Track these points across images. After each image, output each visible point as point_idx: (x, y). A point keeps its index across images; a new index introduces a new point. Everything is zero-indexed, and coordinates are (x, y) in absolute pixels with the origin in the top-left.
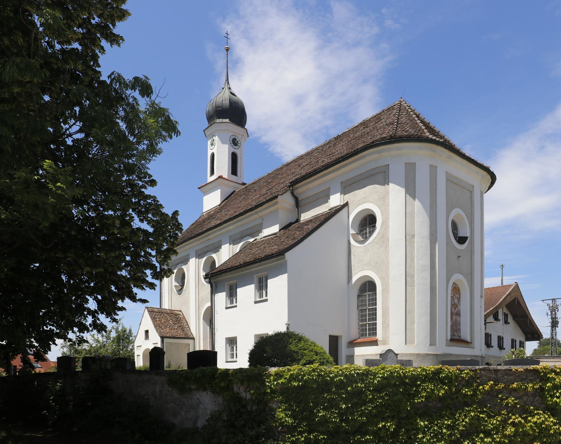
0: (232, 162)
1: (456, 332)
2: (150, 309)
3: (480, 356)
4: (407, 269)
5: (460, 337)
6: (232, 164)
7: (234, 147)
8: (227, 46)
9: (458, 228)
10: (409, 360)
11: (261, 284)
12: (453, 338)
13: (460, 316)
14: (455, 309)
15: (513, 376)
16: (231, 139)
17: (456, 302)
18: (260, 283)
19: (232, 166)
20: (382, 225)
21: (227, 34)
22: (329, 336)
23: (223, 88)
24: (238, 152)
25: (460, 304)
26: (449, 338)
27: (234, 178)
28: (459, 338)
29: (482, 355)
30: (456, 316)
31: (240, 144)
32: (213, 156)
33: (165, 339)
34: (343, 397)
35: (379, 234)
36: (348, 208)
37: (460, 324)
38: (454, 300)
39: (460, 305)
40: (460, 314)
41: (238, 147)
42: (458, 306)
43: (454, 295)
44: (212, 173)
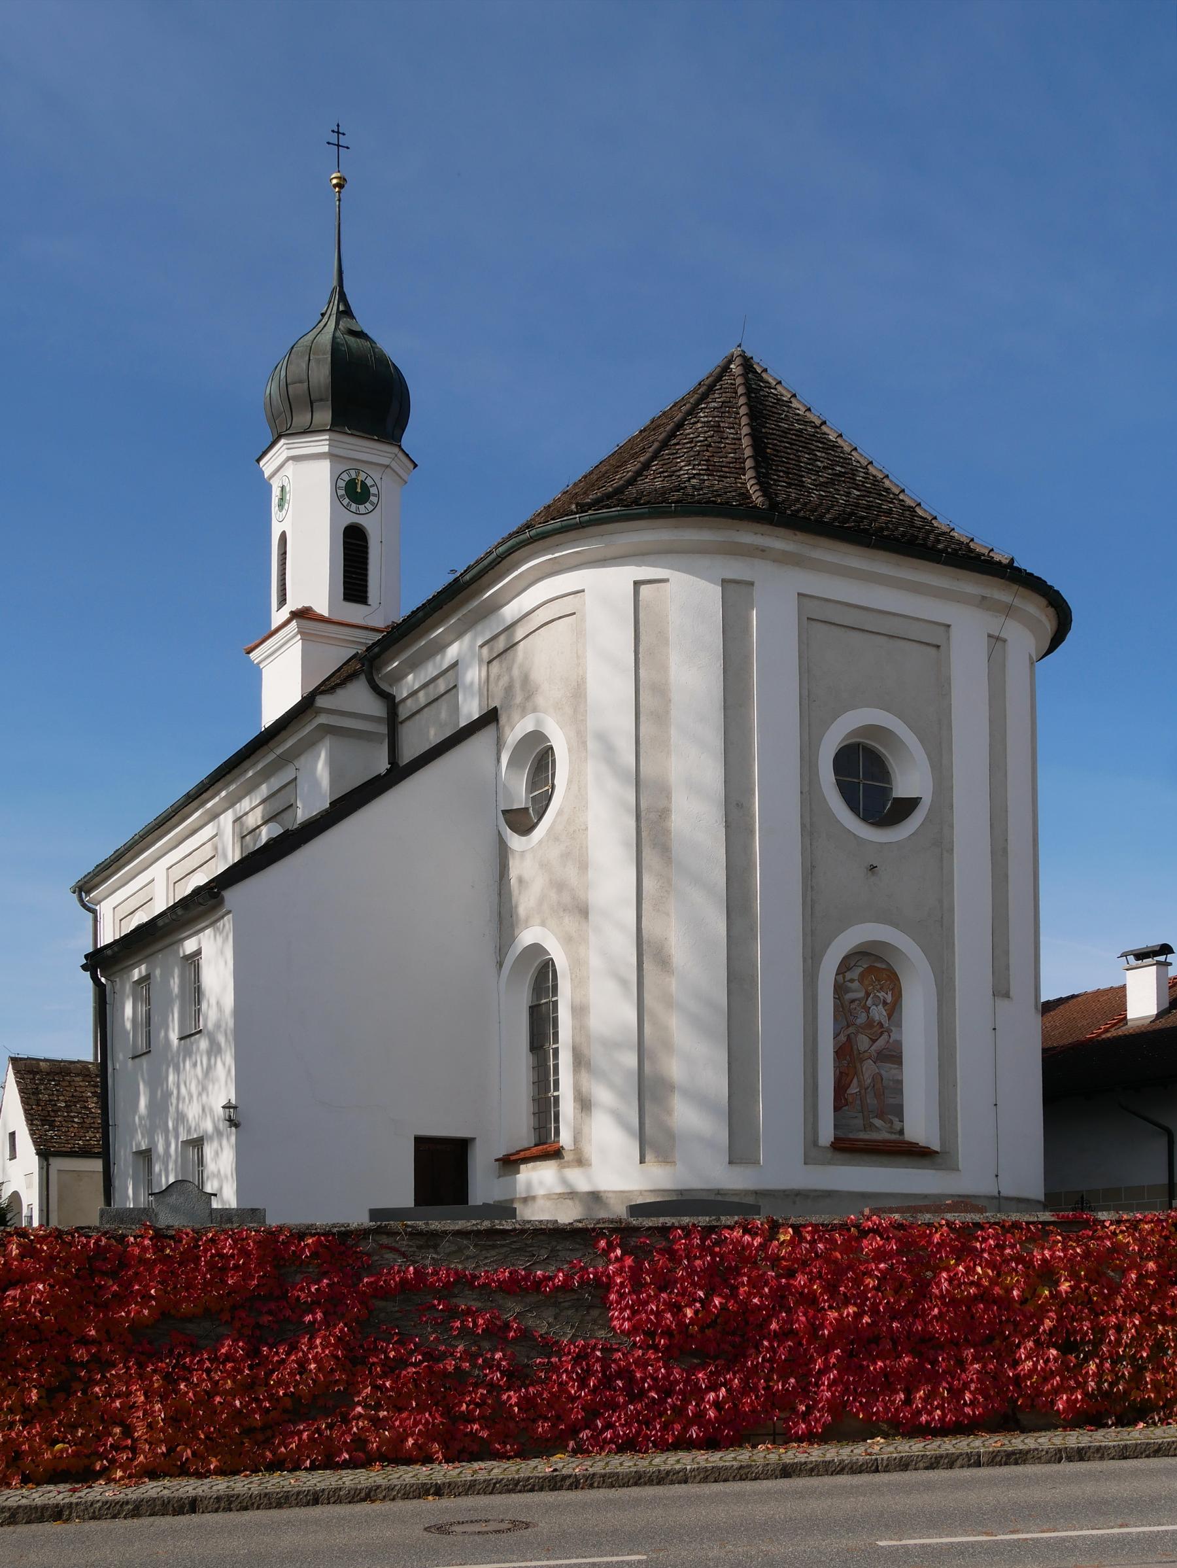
0: (345, 560)
1: (881, 1115)
2: (21, 1065)
3: (993, 1198)
4: (644, 919)
5: (901, 1132)
6: (345, 566)
7: (354, 507)
8: (339, 172)
9: (891, 772)
10: (252, 1209)
11: (196, 985)
12: (841, 1135)
13: (900, 1063)
14: (874, 1041)
15: (497, 1250)
16: (342, 484)
17: (877, 1018)
18: (199, 986)
19: (345, 571)
20: (570, 781)
21: (338, 133)
22: (415, 1138)
23: (323, 315)
24: (371, 523)
25: (901, 1020)
26: (827, 1134)
27: (354, 613)
28: (894, 1137)
29: (999, 1192)
30: (879, 1064)
31: (378, 496)
32: (283, 537)
33: (52, 1160)
34: (122, 1316)
35: (560, 813)
36: (498, 729)
37: (900, 1092)
38: (868, 1012)
39: (899, 1025)
40: (901, 1057)
41: (370, 507)
42: (889, 1031)
43: (868, 995)
44: (282, 601)
